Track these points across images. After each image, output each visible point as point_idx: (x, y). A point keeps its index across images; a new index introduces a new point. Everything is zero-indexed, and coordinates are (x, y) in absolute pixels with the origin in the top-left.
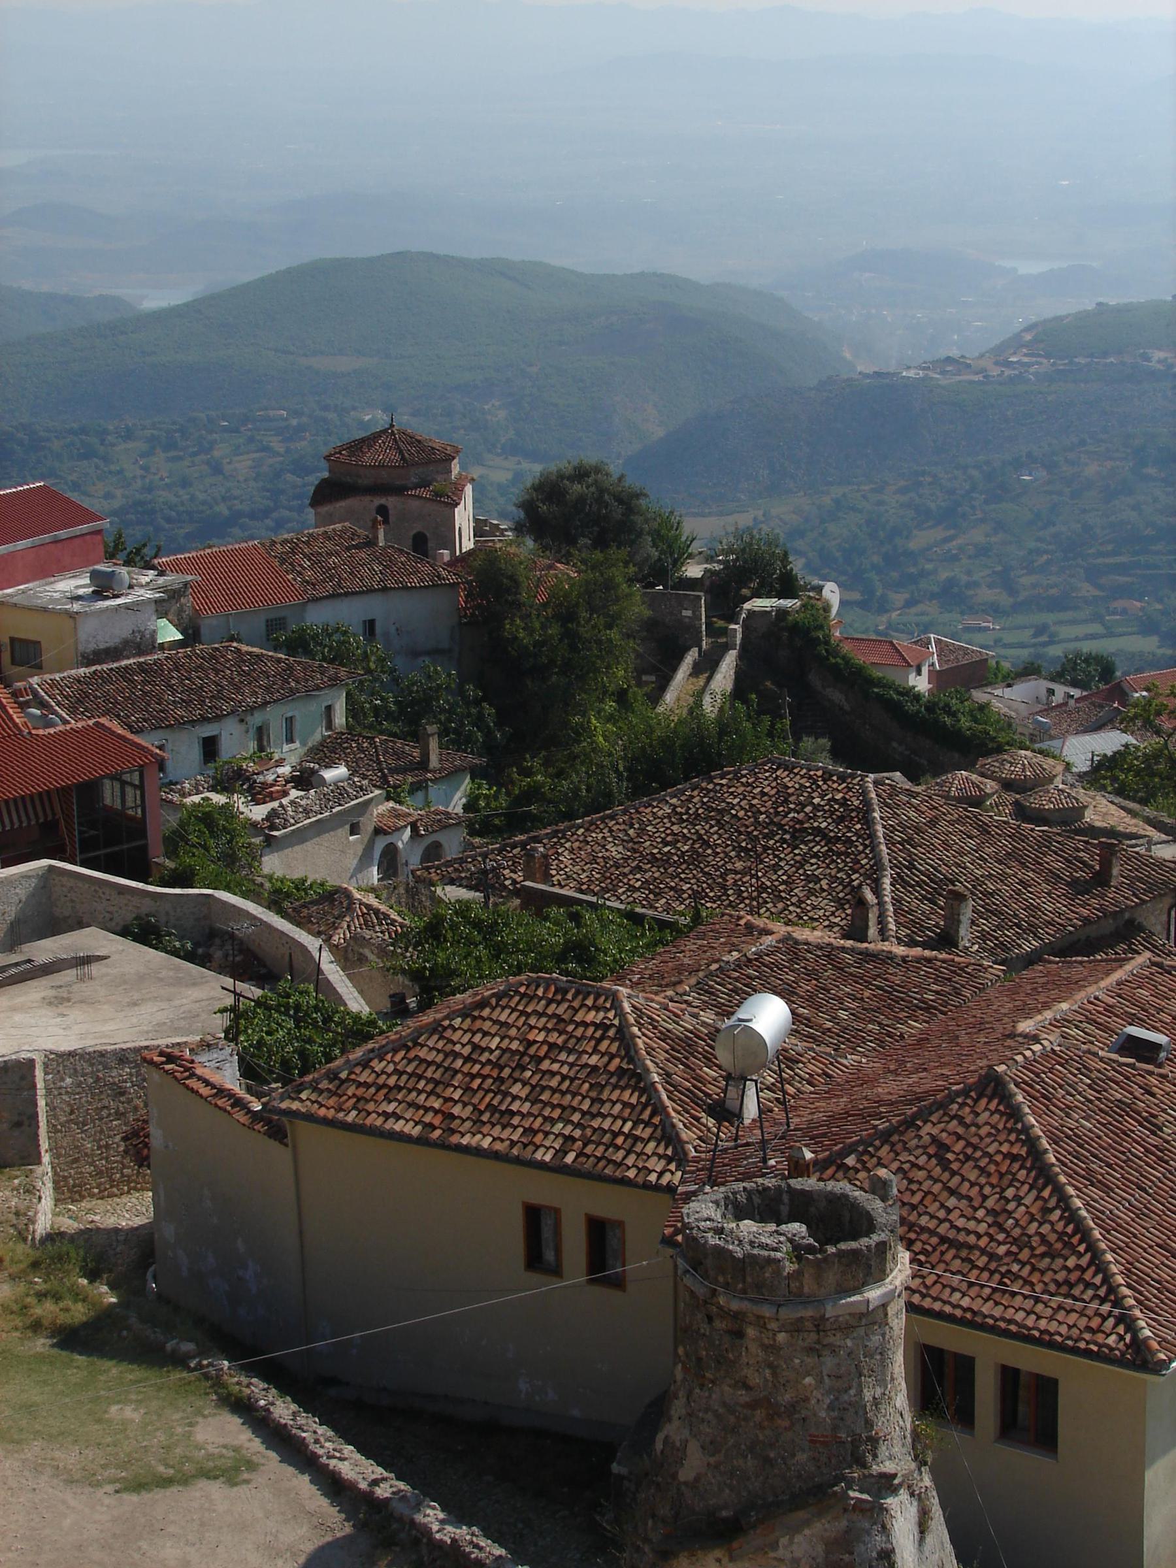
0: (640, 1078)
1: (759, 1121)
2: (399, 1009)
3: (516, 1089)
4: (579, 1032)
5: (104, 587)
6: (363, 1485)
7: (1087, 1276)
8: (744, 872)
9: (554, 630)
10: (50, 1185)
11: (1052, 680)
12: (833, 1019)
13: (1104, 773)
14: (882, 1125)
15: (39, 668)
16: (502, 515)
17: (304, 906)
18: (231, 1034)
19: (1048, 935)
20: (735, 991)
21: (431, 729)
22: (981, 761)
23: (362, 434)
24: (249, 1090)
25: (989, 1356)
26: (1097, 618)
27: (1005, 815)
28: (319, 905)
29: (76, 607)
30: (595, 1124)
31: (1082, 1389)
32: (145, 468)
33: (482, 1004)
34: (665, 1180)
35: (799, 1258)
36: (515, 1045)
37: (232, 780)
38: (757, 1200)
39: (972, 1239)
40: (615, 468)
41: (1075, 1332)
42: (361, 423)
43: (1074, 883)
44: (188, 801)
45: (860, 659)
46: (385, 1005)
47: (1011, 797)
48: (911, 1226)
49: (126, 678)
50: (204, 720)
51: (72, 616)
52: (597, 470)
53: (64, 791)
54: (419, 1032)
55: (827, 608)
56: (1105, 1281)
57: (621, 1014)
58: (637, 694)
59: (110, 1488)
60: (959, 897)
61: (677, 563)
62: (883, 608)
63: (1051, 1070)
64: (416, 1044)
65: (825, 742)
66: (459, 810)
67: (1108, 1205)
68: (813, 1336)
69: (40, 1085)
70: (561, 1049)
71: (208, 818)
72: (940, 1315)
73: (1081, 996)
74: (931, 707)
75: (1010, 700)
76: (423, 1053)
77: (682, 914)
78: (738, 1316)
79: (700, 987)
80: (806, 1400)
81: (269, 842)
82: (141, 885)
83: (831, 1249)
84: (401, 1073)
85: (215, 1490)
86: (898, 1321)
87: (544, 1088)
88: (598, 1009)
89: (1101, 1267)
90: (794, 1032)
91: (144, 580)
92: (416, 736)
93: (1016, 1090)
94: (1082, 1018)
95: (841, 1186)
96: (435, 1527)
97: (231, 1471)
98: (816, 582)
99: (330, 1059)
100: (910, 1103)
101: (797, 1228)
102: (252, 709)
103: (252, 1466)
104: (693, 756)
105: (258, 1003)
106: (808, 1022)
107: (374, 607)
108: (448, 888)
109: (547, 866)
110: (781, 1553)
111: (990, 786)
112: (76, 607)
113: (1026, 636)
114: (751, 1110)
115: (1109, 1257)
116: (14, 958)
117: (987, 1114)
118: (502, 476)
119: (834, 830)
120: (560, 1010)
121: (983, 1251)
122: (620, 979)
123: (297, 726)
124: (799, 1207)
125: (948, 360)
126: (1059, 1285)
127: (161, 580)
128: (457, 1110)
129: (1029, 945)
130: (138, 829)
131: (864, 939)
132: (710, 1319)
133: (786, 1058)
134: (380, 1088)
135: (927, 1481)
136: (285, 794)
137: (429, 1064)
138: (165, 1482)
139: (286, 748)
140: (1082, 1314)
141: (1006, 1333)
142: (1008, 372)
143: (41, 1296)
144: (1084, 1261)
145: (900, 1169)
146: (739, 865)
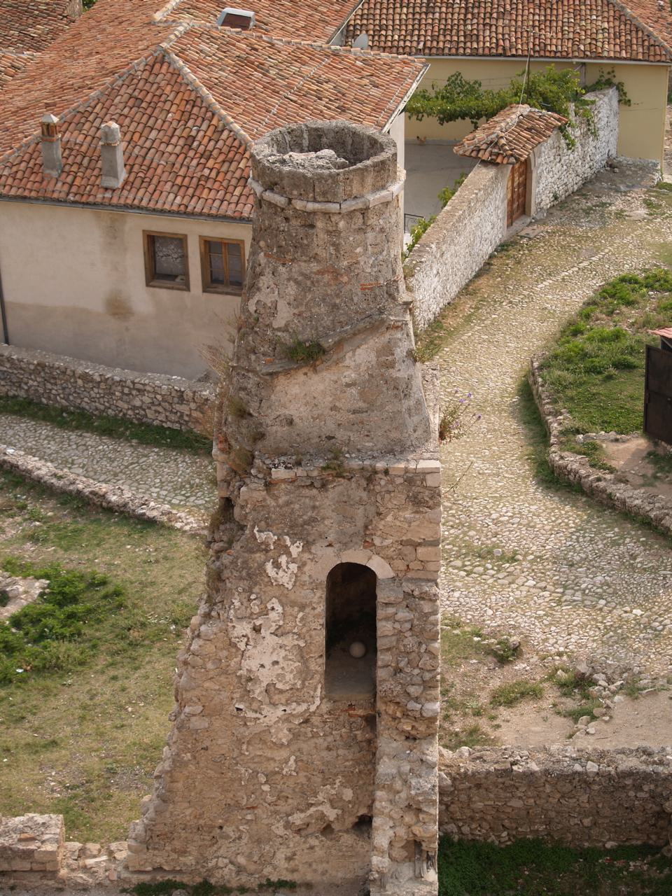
78: (314, 213)
93: (177, 58)
94: (189, 6)
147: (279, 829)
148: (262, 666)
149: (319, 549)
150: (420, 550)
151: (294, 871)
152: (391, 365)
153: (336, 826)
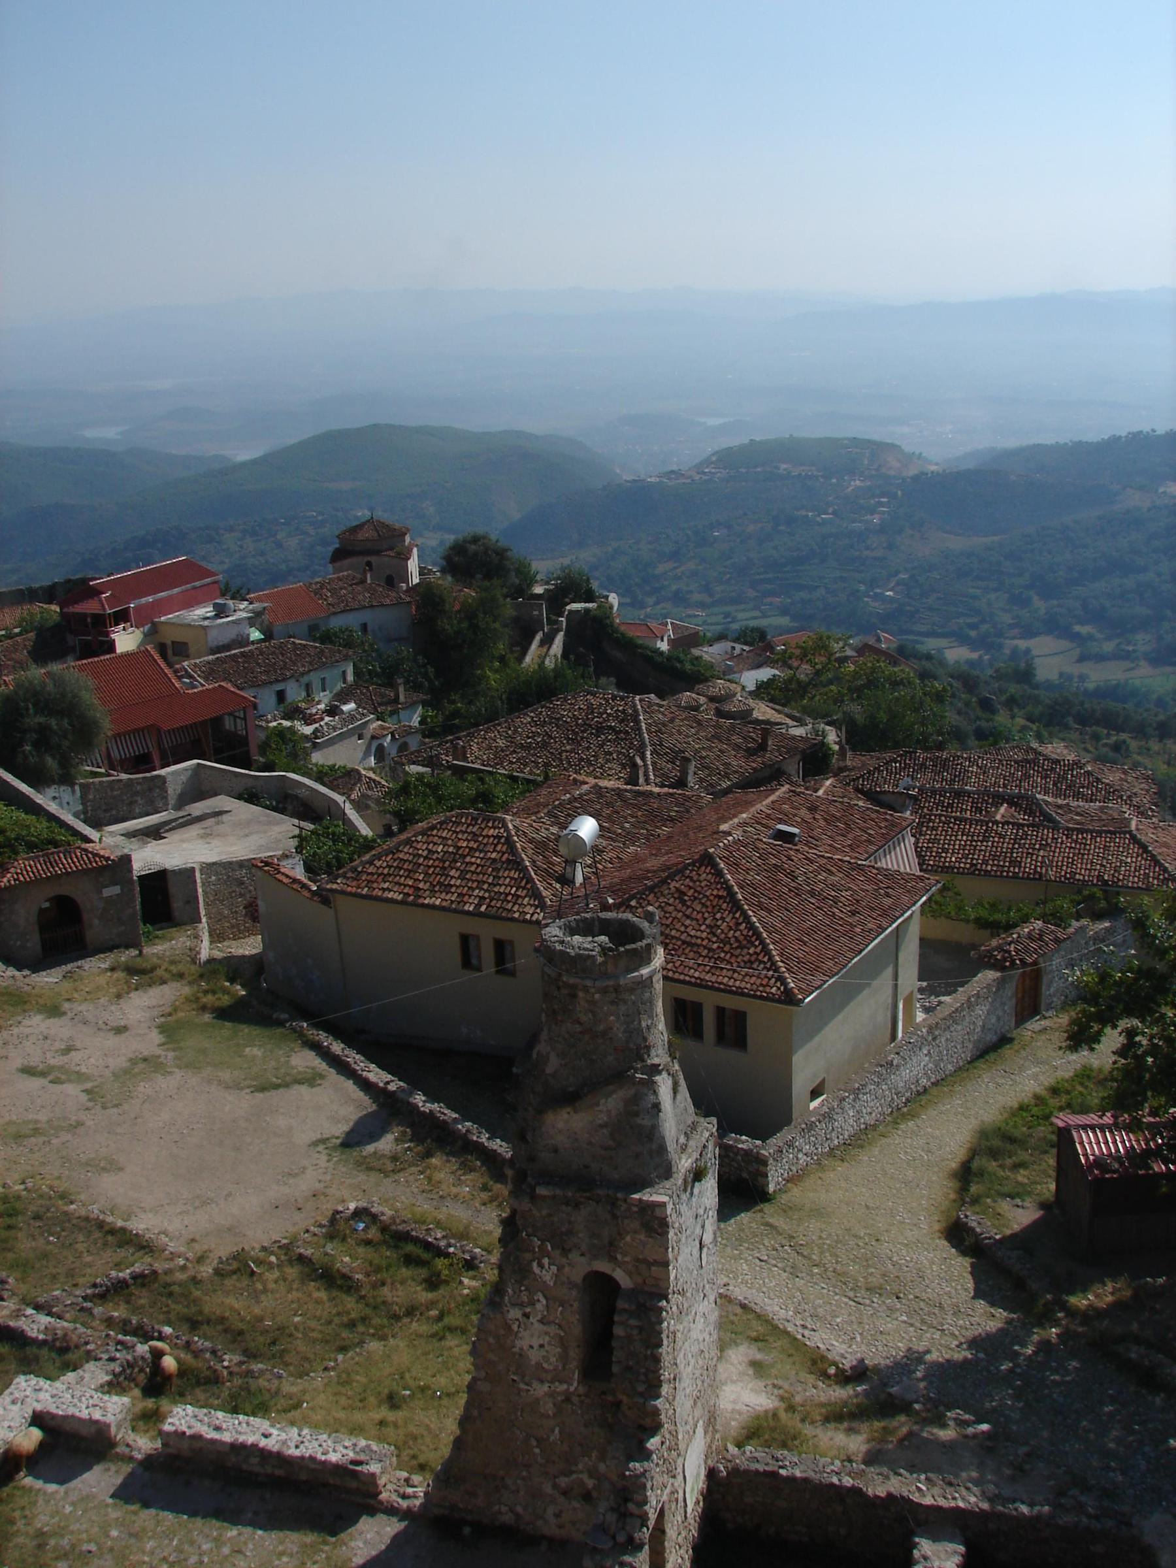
0: (519, 864)
1: (584, 884)
2: (388, 833)
3: (452, 873)
4: (485, 841)
5: (221, 611)
6: (381, 1085)
7: (760, 957)
8: (571, 751)
9: (465, 625)
10: (207, 934)
11: (734, 641)
12: (622, 828)
13: (763, 690)
14: (649, 883)
15: (187, 657)
16: (434, 565)
17: (335, 779)
18: (299, 849)
19: (735, 778)
20: (569, 815)
21: (399, 681)
22: (697, 686)
23: (354, 524)
24: (310, 879)
25: (709, 1002)
26: (757, 608)
27: (711, 715)
28: (343, 778)
29: (206, 623)
30: (496, 889)
31: (759, 1017)
32: (241, 547)
33: (433, 828)
34: (534, 918)
35: (605, 954)
36: (451, 850)
37: (293, 713)
38: (581, 925)
39: (699, 941)
40: (493, 537)
41: (755, 987)
42: (357, 518)
43: (748, 750)
44: (271, 725)
45: (631, 633)
46: (381, 831)
47: (713, 705)
48: (667, 936)
49: (233, 659)
50: (277, 681)
51: (204, 628)
52: (484, 537)
53: (203, 723)
54: (399, 844)
55: (611, 607)
56: (770, 959)
57: (507, 830)
58: (511, 658)
59: (248, 1091)
60: (687, 760)
61: (530, 586)
62: (642, 607)
63: (738, 850)
64: (398, 851)
65: (613, 679)
66: (417, 724)
67: (770, 919)
68: (614, 995)
69: (199, 881)
70: (476, 850)
71: (281, 733)
72: (683, 982)
73: (753, 810)
74: (669, 658)
75: (711, 653)
76: (401, 855)
77: (539, 775)
78: (574, 987)
79: (549, 814)
80: (611, 1029)
81: (315, 746)
82: (247, 772)
83: (622, 949)
84: (390, 867)
85: (303, 1089)
86: (658, 985)
87: (468, 872)
88: (495, 828)
89: (767, 952)
90: (601, 836)
91: (242, 607)
92: (392, 685)
95: (628, 916)
96: (420, 1104)
97: (312, 1080)
98: (606, 593)
99: (352, 860)
100: (663, 871)
101: (603, 939)
102: (302, 674)
103: (322, 1077)
104: (539, 691)
105: (312, 832)
106: (609, 830)
107: (366, 616)
108: (412, 767)
109: (465, 753)
110: (601, 1108)
111: (702, 700)
112: (206, 623)
113: (719, 619)
114: (579, 879)
115: (771, 947)
116: (181, 814)
117: (705, 875)
118: (434, 543)
119: (619, 727)
120: (475, 830)
121: (705, 947)
122: (506, 812)
123: (328, 682)
124: (605, 927)
125: (672, 472)
126: (745, 962)
127: (251, 607)
128: (421, 885)
129: (726, 784)
130: (243, 741)
131: (637, 785)
132: (559, 988)
133: (597, 850)
134: (379, 875)
135: (677, 1067)
136: (322, 719)
137: (405, 861)
138: (277, 1087)
139: (322, 694)
140: (758, 977)
141: (719, 990)
142: (705, 478)
143: (206, 992)
144: (758, 950)
145: (660, 906)
146: (568, 748)
147: (548, 1488)
148: (531, 1347)
149: (574, 1256)
150: (653, 1268)
151: (561, 1527)
152: (637, 1114)
153: (594, 1494)
